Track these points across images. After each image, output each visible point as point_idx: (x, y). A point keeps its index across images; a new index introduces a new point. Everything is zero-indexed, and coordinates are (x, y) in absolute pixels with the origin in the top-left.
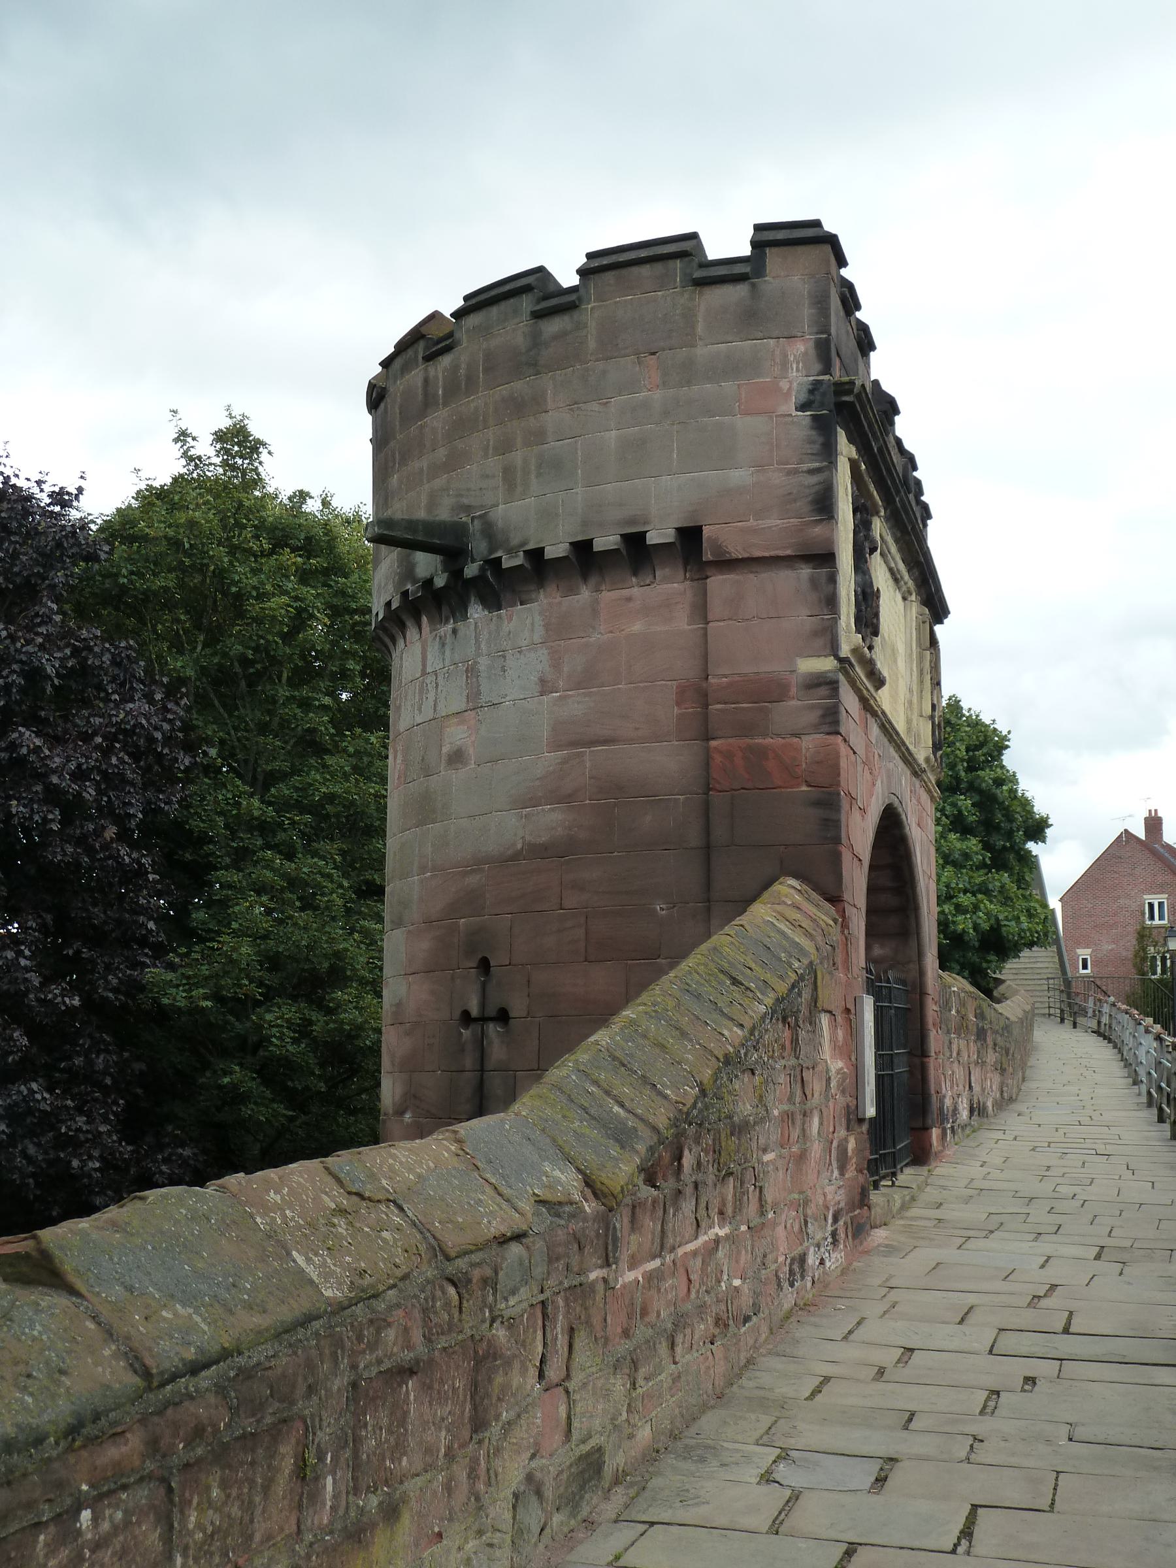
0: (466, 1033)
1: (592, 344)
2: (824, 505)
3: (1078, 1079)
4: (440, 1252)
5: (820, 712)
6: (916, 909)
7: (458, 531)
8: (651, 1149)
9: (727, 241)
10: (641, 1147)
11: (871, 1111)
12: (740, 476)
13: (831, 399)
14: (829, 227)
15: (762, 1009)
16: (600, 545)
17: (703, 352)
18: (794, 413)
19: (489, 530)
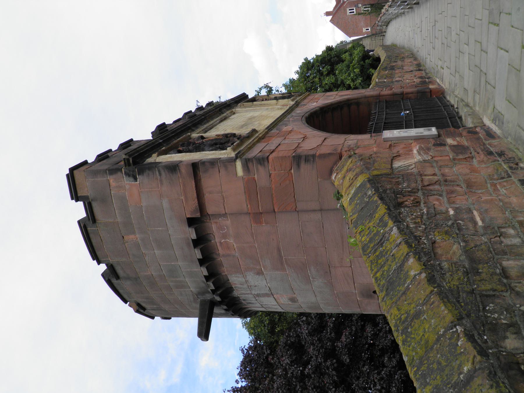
1: (124, 259)
2: (173, 168)
3: (403, 31)
5: (259, 166)
6: (348, 100)
7: (203, 303)
11: (434, 131)
12: (165, 204)
13: (132, 167)
14: (68, 172)
15: (395, 230)
16: (200, 256)
17: (119, 219)
18: (138, 182)
19: (203, 293)
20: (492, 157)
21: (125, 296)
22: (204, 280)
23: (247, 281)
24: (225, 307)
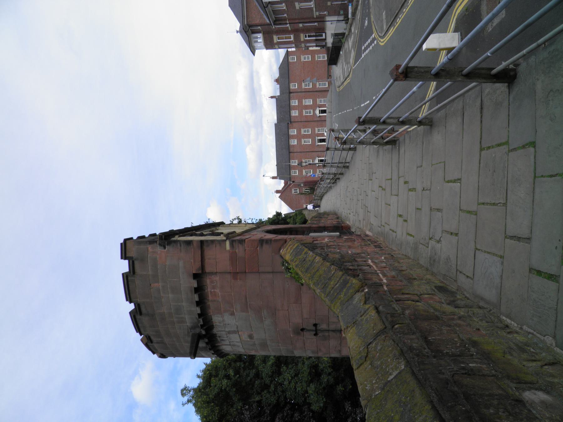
0: (320, 334)
2: (189, 243)
4: (383, 332)
7: (193, 336)
8: (348, 275)
9: (125, 266)
10: (348, 278)
11: (338, 233)
12: (181, 264)
14: (122, 242)
17: (150, 273)
19: (193, 328)
22: (197, 317)
23: (223, 320)
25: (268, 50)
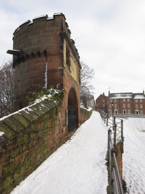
2: (62, 48)
9: (51, 16)
14: (63, 14)
17: (47, 29)
20: (60, 139)
21: (21, 27)
24: (17, 59)
25: (106, 187)
